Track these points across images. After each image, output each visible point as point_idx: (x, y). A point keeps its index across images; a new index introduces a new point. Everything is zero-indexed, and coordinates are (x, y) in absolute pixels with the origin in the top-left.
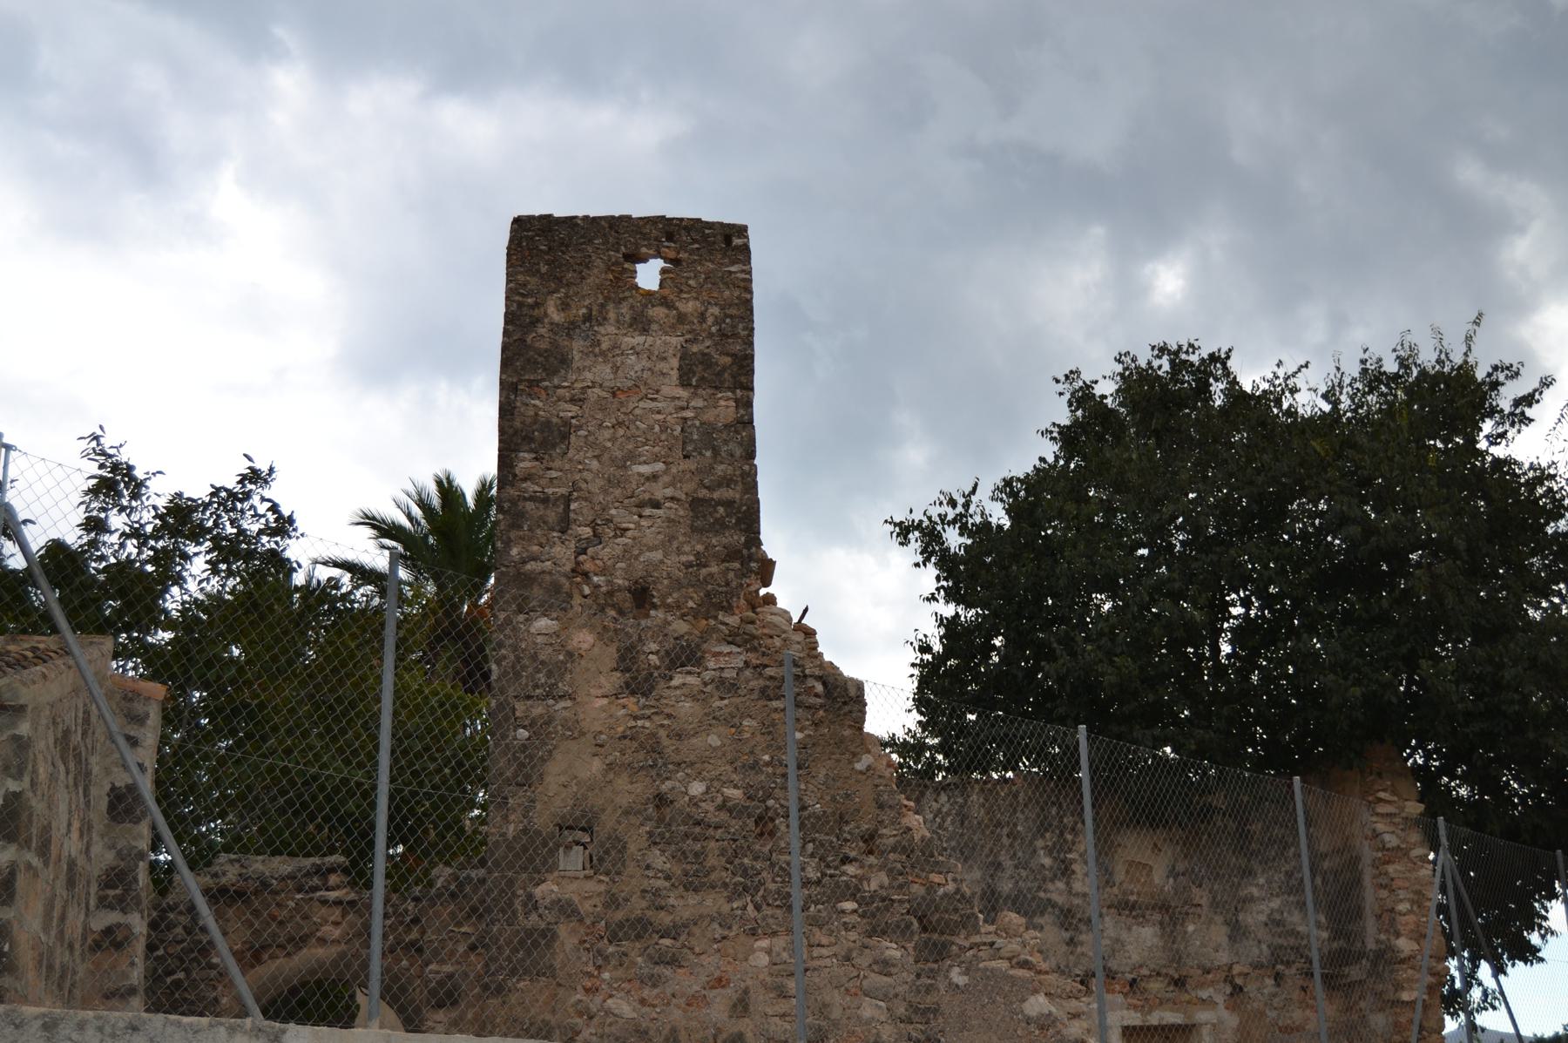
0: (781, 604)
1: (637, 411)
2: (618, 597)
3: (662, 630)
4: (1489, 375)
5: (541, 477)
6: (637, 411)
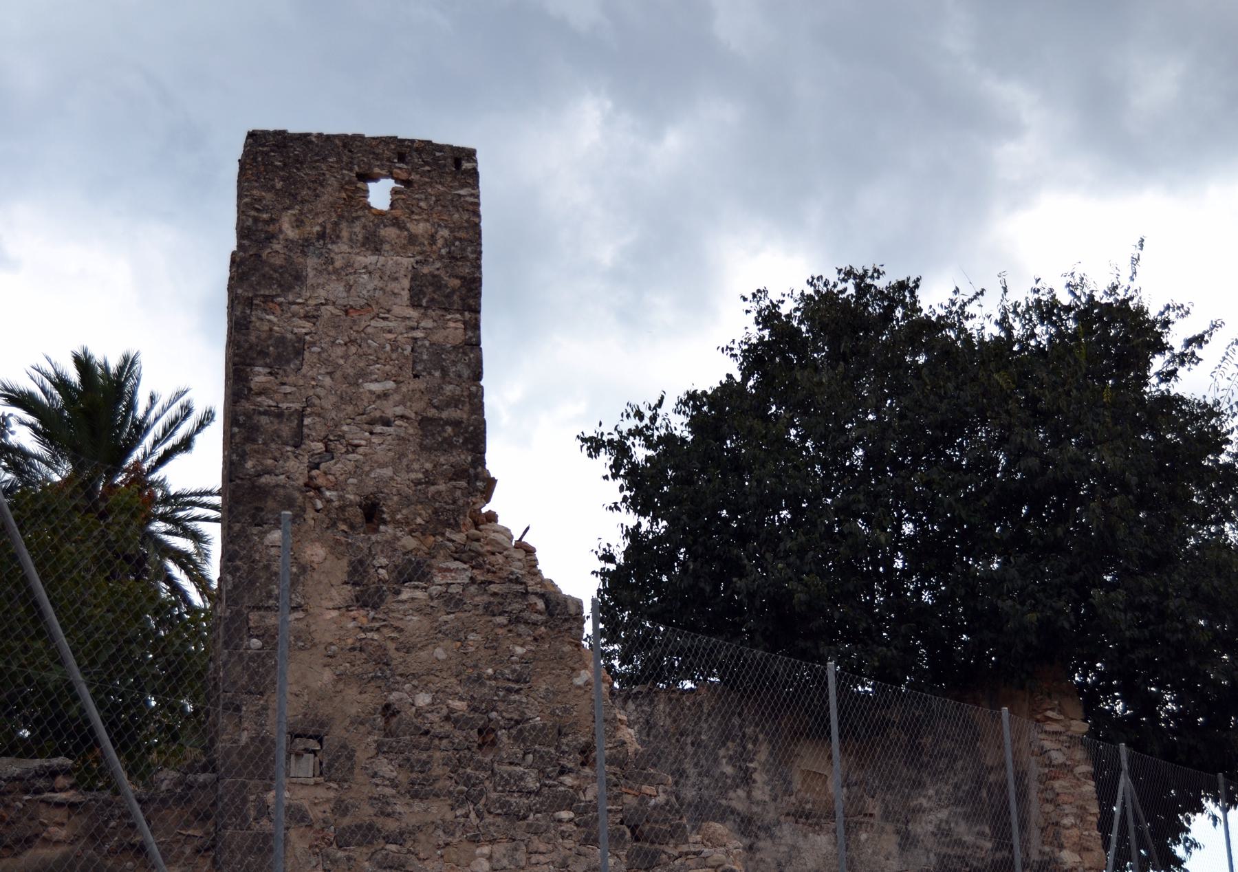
0: (502, 522)
1: (369, 330)
2: (350, 512)
3: (391, 544)
4: (1162, 313)
5: (275, 392)
6: (369, 330)
